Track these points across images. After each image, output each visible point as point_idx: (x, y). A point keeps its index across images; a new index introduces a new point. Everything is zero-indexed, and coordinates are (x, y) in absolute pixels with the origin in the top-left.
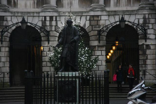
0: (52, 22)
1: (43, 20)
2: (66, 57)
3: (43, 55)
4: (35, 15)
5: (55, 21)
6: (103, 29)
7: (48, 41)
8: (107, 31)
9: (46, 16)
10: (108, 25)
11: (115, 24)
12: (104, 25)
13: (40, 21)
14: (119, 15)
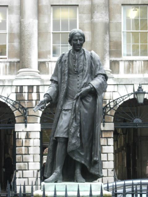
0: (31, 94)
1: (19, 91)
2: (66, 140)
3: (17, 145)
4: (6, 84)
5: (37, 92)
6: (110, 106)
7: (25, 122)
8: (116, 109)
9: (22, 86)
10: (118, 99)
11: (128, 99)
12: (110, 99)
13: (13, 93)
14: (133, 84)
